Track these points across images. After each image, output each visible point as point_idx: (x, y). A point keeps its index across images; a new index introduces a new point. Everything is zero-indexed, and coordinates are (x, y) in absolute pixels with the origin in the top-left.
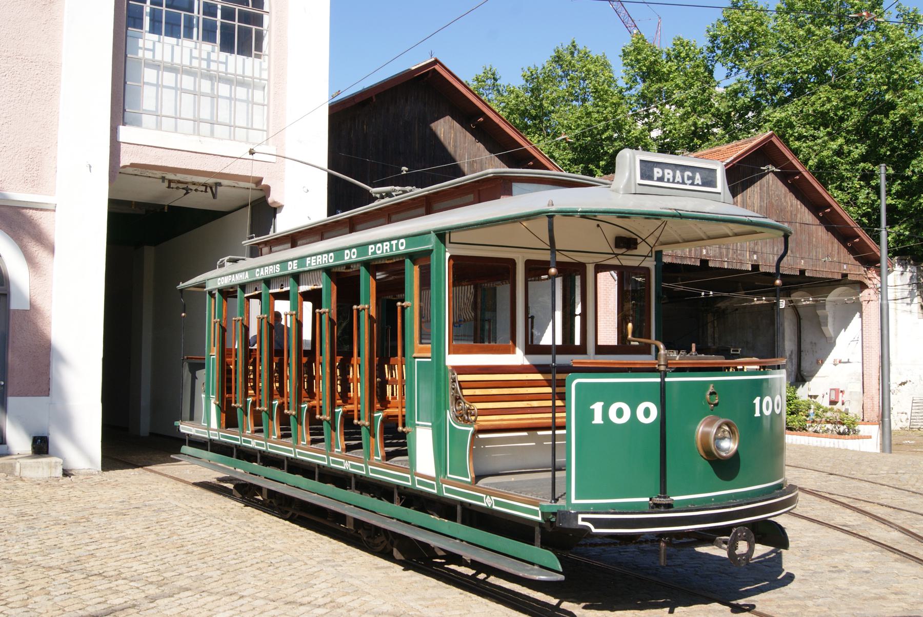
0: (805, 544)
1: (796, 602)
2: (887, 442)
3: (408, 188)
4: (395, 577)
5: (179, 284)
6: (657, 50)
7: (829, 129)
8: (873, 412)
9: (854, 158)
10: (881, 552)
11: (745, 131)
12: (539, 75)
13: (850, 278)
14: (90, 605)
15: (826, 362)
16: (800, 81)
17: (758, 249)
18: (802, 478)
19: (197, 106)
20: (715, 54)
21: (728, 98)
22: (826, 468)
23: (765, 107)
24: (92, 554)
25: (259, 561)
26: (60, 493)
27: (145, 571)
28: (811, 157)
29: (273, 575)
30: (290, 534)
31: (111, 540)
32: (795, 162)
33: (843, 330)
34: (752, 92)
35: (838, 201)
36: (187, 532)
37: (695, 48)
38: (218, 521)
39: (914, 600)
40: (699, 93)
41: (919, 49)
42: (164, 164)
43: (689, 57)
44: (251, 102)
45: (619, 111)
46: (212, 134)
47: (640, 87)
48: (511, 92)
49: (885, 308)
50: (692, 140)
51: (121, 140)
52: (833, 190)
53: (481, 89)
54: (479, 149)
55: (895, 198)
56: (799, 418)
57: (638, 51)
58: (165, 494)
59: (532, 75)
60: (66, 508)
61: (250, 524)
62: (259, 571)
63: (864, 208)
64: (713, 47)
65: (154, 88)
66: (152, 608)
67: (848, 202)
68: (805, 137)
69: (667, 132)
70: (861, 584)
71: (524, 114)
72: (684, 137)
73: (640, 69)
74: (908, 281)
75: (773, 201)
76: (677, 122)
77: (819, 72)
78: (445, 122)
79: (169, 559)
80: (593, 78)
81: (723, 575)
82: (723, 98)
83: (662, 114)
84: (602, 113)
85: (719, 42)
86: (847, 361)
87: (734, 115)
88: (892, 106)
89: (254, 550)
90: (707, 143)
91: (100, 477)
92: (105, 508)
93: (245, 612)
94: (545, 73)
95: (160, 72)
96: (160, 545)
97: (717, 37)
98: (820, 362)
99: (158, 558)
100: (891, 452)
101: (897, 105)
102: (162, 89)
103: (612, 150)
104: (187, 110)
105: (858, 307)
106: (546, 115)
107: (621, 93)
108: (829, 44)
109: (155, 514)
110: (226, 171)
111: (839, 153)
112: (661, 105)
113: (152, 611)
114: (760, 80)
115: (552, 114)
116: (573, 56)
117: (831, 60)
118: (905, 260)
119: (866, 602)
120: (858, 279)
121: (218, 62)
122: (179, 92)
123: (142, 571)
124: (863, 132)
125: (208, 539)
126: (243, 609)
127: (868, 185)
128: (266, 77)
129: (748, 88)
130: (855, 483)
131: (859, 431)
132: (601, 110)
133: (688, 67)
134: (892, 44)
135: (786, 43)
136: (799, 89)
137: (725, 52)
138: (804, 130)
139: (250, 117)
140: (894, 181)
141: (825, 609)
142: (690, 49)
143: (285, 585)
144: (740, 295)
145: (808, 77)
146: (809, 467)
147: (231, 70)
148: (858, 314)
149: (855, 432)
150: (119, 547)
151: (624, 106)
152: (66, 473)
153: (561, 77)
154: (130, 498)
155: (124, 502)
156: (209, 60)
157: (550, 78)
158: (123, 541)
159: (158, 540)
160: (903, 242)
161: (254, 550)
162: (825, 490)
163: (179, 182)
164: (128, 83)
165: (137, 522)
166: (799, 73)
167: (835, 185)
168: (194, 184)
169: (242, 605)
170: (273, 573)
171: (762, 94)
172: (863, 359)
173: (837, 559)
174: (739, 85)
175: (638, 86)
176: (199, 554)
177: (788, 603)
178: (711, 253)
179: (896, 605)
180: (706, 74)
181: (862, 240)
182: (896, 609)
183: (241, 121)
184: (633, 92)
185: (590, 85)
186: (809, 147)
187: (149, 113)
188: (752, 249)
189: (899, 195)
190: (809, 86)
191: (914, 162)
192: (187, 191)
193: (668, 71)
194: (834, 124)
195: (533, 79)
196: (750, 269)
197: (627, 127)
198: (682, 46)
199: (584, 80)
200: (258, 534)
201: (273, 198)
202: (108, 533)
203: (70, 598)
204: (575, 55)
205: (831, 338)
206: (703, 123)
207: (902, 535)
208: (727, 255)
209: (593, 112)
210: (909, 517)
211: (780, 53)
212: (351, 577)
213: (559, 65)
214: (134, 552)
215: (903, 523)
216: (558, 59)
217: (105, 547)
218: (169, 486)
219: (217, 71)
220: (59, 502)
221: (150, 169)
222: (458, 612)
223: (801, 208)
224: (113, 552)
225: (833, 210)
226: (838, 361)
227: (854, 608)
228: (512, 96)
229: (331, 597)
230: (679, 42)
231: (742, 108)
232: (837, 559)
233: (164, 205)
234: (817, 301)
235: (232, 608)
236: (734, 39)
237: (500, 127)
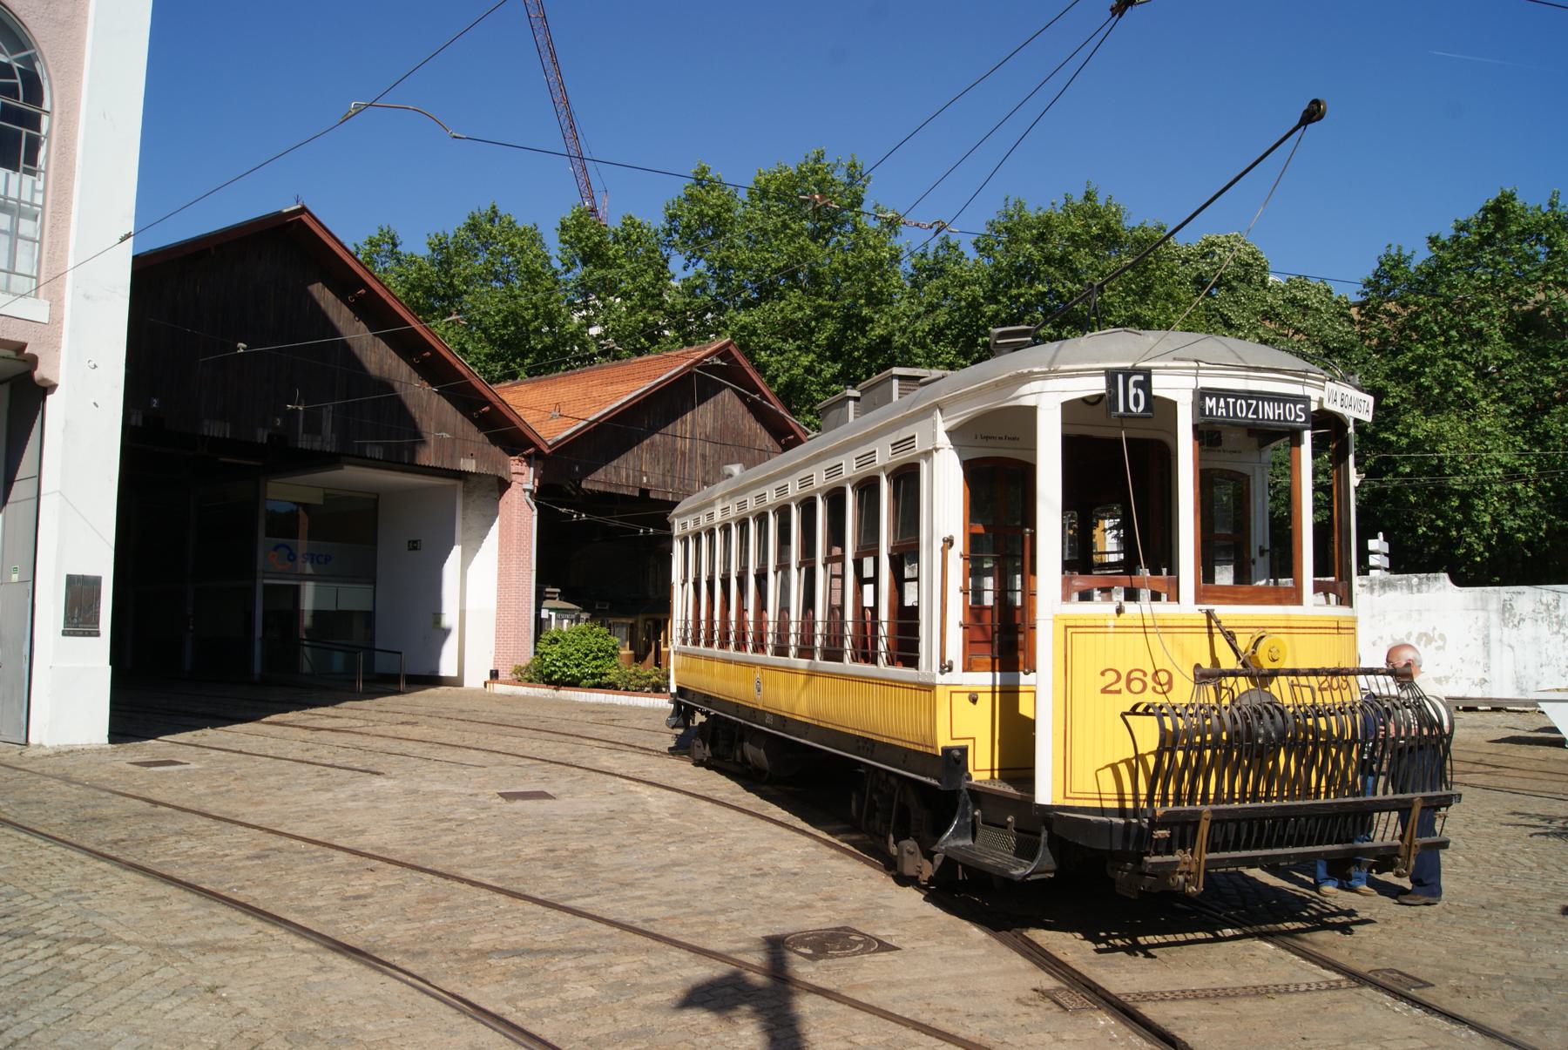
1: (705, 918)
4: (166, 912)
10: (816, 847)
37: (649, 230)
47: (579, 271)
53: (375, 256)
59: (441, 244)
64: (670, 229)
70: (786, 890)
71: (429, 292)
73: (581, 249)
111: (809, 370)
119: (789, 913)
128: (40, 203)
136: (767, 292)
141: (739, 925)
157: (462, 250)
175: (576, 270)
177: (694, 919)
179: (823, 914)
184: (570, 275)
208: (672, 486)
212: (101, 914)
216: (473, 227)
227: (773, 922)
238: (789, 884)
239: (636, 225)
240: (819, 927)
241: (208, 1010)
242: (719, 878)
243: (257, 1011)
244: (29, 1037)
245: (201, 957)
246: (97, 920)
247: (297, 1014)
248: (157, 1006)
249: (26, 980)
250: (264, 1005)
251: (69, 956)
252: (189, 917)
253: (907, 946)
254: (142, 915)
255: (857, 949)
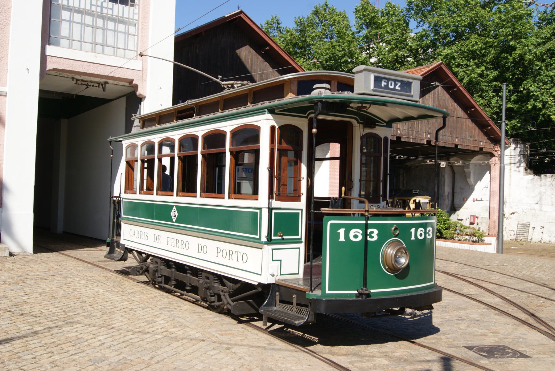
0: (445, 304)
2: (500, 247)
3: (245, 82)
4: (204, 318)
5: (109, 138)
6: (376, 9)
7: (476, 61)
8: (495, 231)
9: (490, 79)
10: (488, 309)
11: (426, 60)
12: (305, 22)
13: (484, 150)
14: (23, 330)
15: (468, 200)
16: (460, 32)
17: (431, 131)
18: (448, 266)
19: (94, 35)
20: (410, 13)
21: (417, 40)
22: (462, 261)
23: (439, 46)
24: (26, 302)
25: (125, 307)
26: (7, 266)
27: (57, 312)
28: (464, 77)
29: (133, 315)
30: (144, 292)
31: (37, 294)
32: (454, 80)
33: (479, 181)
34: (432, 37)
35: (480, 104)
36: (83, 290)
37: (399, 9)
38: (102, 284)
39: (502, 336)
40: (400, 36)
41: (531, 15)
42: (73, 69)
43: (394, 14)
44: (127, 33)
45: (352, 46)
46: (103, 52)
47: (365, 31)
48: (288, 32)
49: (502, 168)
50: (395, 65)
51: (47, 54)
52: (477, 98)
53: (270, 30)
54: (266, 66)
55: (513, 104)
56: (450, 232)
57: (365, 9)
58: (71, 268)
59: (301, 22)
60: (11, 274)
61: (121, 287)
62: (124, 313)
63: (495, 109)
64: (409, 9)
65: (68, 23)
66: (60, 333)
67: (485, 105)
68: (461, 65)
69: (380, 59)
70: (474, 327)
71: (295, 45)
72: (390, 62)
73: (365, 20)
74: (518, 153)
75: (441, 103)
76: (386, 53)
77: (472, 26)
78: (246, 49)
79: (71, 305)
80: (337, 25)
81: (396, 321)
82: (414, 40)
83: (377, 48)
84: (342, 46)
85: (413, 6)
86: (480, 199)
87: (420, 51)
88: (514, 49)
89: (122, 301)
90: (404, 67)
91: (32, 257)
92: (34, 275)
93: (115, 336)
94: (308, 21)
95: (72, 13)
96: (67, 297)
97: (412, 3)
98: (465, 199)
99: (65, 305)
100: (502, 253)
101: (516, 48)
102: (73, 24)
103: (346, 69)
104: (88, 37)
105: (488, 168)
106: (308, 46)
107: (353, 35)
108: (478, 9)
109: (64, 279)
110: (111, 75)
111: (481, 75)
112: (377, 43)
113: (60, 334)
114: (437, 30)
115: (312, 46)
116: (325, 11)
117: (479, 19)
118: (518, 140)
119: (475, 337)
120: (489, 151)
121: (108, 8)
122: (83, 26)
123: (55, 312)
124: (496, 64)
125: (95, 294)
126: (114, 334)
127: (498, 95)
128: (137, 19)
129: (429, 34)
130: (478, 270)
131: (484, 240)
132: (341, 44)
133: (394, 20)
134: (516, 11)
135: (452, 8)
136: (459, 36)
137: (416, 12)
138: (461, 61)
139: (126, 42)
140: (513, 93)
141: (451, 340)
142: (395, 9)
143: (139, 321)
144: (420, 158)
145: (465, 29)
146: (453, 261)
147: (115, 13)
148: (488, 172)
149: (482, 241)
150: (42, 297)
151: (355, 43)
152: (11, 255)
153: (318, 23)
154: (49, 270)
155: (45, 271)
156: (102, 7)
157: (311, 24)
158: (44, 294)
159: (65, 294)
160: (516, 130)
161: (122, 301)
162: (460, 274)
163: (83, 81)
164: (52, 19)
165: (53, 284)
166: (460, 27)
167: (478, 94)
168: (92, 82)
169: (114, 332)
170: (132, 314)
171: (437, 39)
172: (490, 199)
173: (462, 313)
174: (424, 33)
175: (363, 31)
176: (90, 303)
178: (403, 133)
179: (492, 339)
180: (405, 25)
181: (492, 128)
182: (492, 341)
183: (121, 45)
184: (361, 34)
185: (335, 29)
186: (464, 72)
187: (65, 38)
188: (428, 131)
189: (515, 102)
190: (465, 34)
191: (525, 82)
192: (88, 86)
193: (382, 22)
194: (479, 58)
195: (301, 24)
196: (426, 143)
197: (356, 56)
198: (391, 7)
199: (332, 26)
200: (125, 292)
201: (140, 92)
202: (35, 290)
203: (11, 326)
204: (327, 11)
205: (472, 185)
206: (401, 54)
207: (501, 300)
208: (412, 134)
209: (336, 45)
210: (506, 290)
211: (449, 14)
212: (179, 317)
213: (317, 16)
214: (51, 300)
215: (502, 293)
216: (316, 13)
217: (33, 298)
218: (73, 263)
219: (107, 14)
220: (6, 271)
221: (64, 72)
222: (240, 338)
223: (457, 108)
224: (38, 301)
225: (476, 109)
226: (476, 199)
227: (467, 340)
228: (288, 34)
229: (166, 328)
230: (389, 5)
231: (425, 46)
232: (462, 313)
233: (74, 94)
234: (464, 163)
235: (107, 333)
236: (422, 4)
237: (279, 53)
238: (475, 325)
239: (392, 6)
240: (490, 345)
241: (228, 356)
242: (441, 320)
243: (247, 358)
244: (163, 360)
245: (221, 336)
246: (179, 319)
247: (263, 361)
248: (208, 353)
249: (157, 340)
250: (250, 356)
251: (171, 332)
252: (213, 320)
253: (534, 356)
254: (195, 319)
255: (509, 355)
